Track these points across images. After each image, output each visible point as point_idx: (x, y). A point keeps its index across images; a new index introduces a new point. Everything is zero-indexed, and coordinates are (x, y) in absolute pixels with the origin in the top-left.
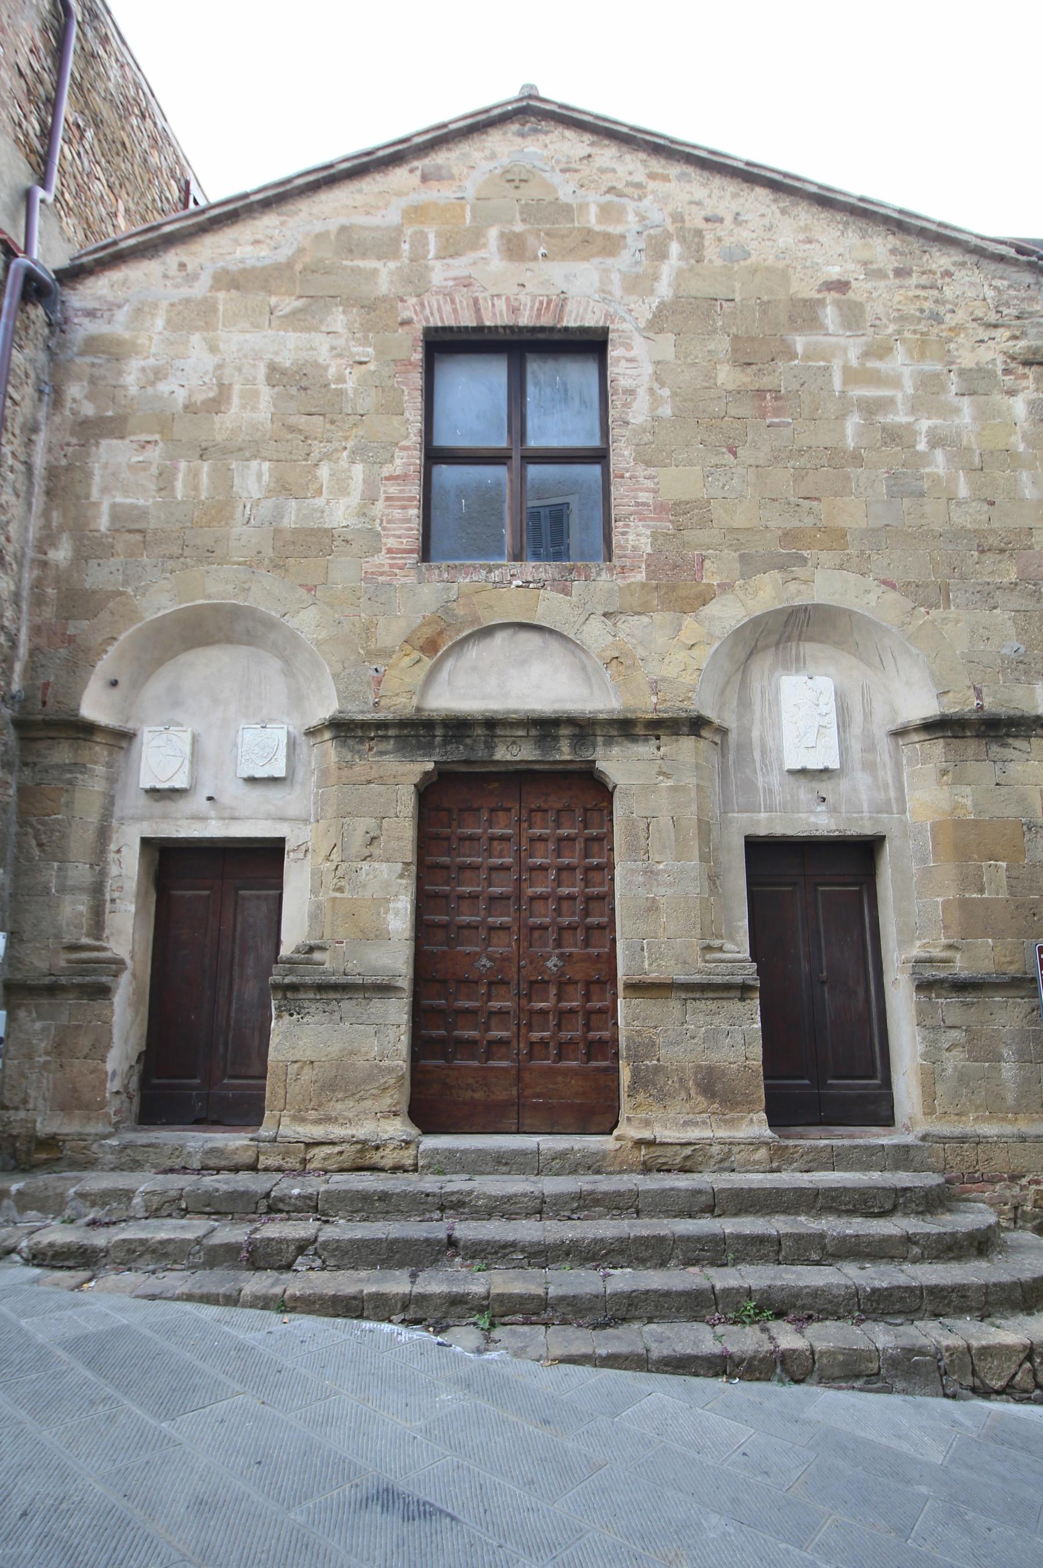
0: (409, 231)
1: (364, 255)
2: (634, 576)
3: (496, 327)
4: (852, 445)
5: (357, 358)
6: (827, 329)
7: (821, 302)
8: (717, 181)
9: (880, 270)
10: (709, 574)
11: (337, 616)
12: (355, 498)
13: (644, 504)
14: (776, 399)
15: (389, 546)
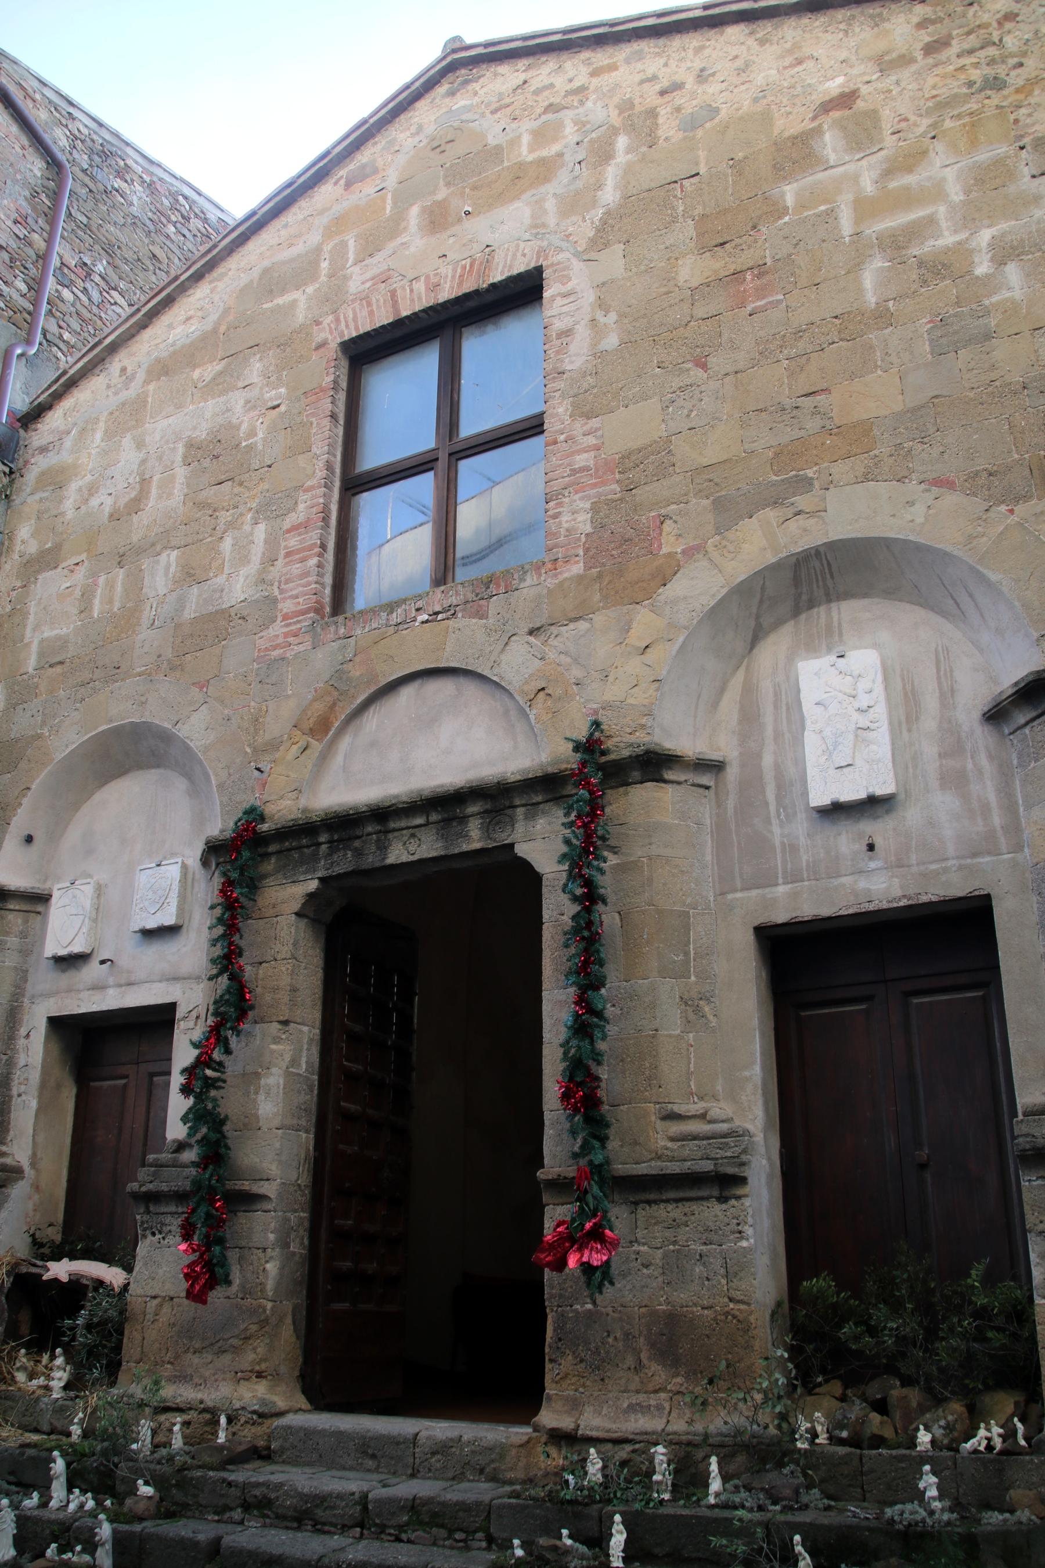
0: (327, 248)
1: (283, 291)
2: (569, 570)
3: (415, 314)
4: (873, 300)
5: (270, 404)
6: (827, 161)
7: (818, 131)
8: (677, 42)
9: (903, 56)
10: (672, 539)
11: (226, 712)
12: (253, 567)
13: (583, 469)
14: (759, 276)
15: (285, 610)
